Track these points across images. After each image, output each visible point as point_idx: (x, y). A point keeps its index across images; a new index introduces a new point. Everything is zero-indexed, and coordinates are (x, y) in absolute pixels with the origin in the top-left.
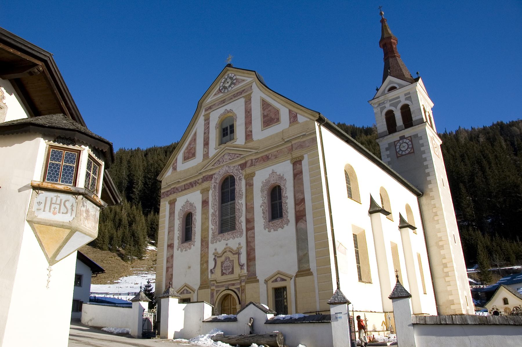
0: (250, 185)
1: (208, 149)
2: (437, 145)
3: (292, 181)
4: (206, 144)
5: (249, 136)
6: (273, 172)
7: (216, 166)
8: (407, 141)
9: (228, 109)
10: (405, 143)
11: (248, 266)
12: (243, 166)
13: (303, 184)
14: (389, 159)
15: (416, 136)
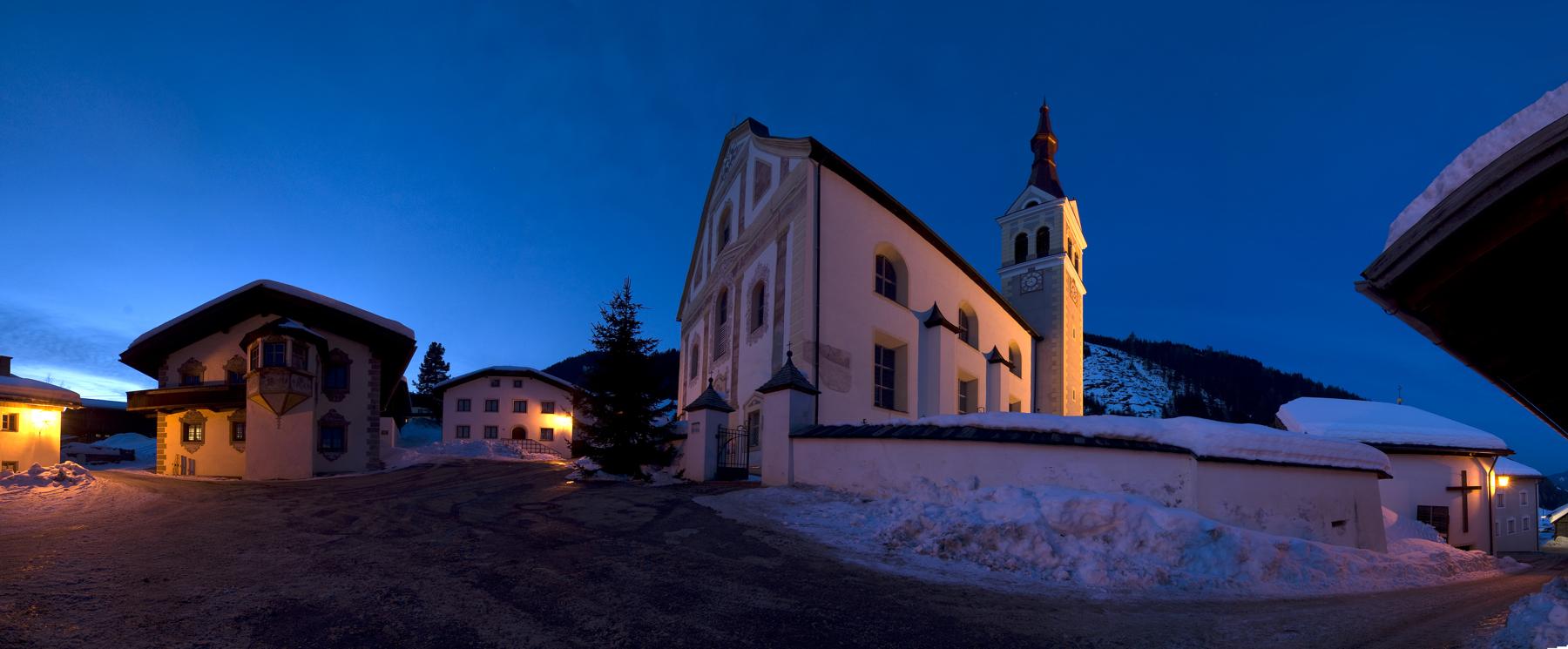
0: (739, 292)
2: (1077, 292)
8: (1038, 275)
12: (734, 271)
15: (1049, 270)
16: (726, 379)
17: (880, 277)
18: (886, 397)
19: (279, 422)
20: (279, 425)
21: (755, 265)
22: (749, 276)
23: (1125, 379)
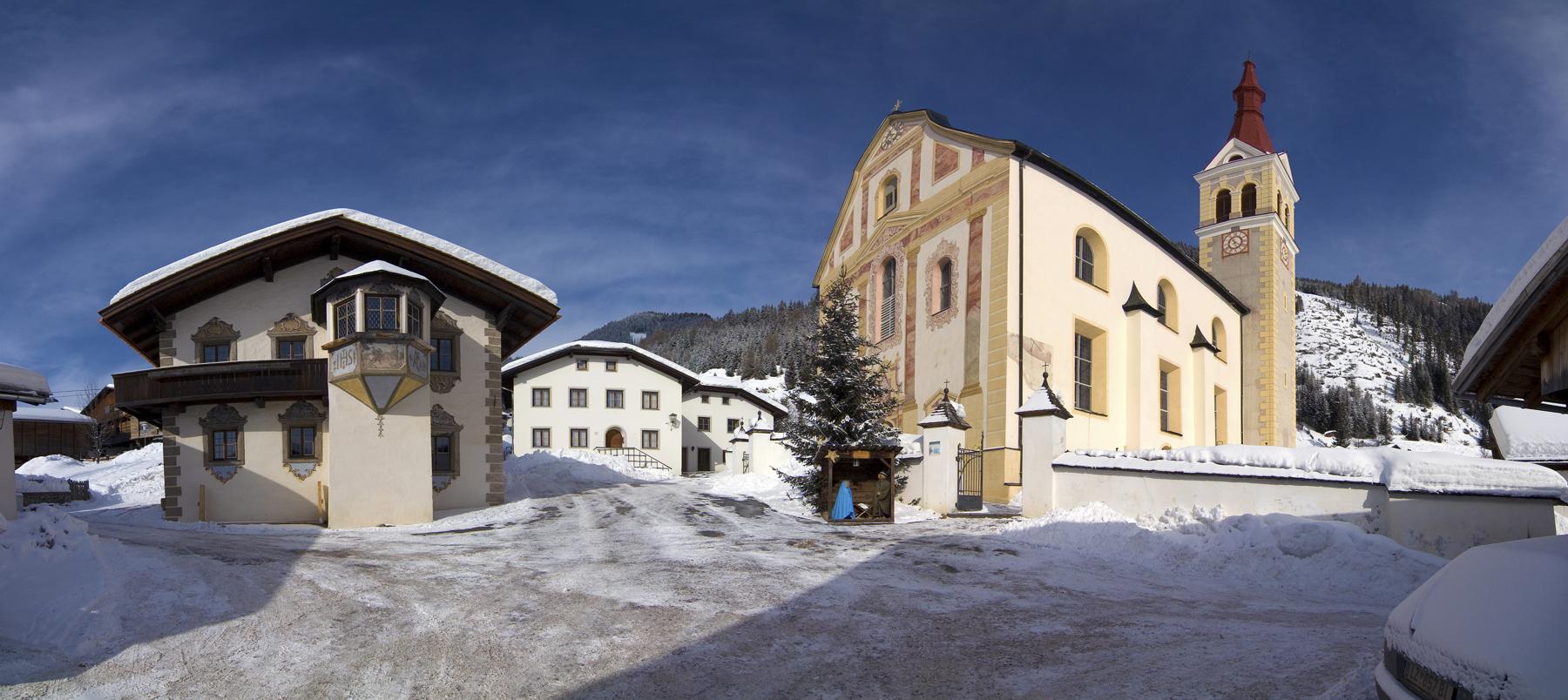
0: (912, 266)
1: (866, 228)
2: (1289, 253)
3: (967, 252)
4: (864, 222)
5: (915, 197)
6: (943, 241)
7: (875, 249)
8: (1242, 235)
9: (891, 169)
10: (1239, 237)
11: (906, 385)
12: (906, 241)
13: (980, 251)
14: (1210, 260)
16: (896, 368)
19: (381, 424)
20: (381, 430)
21: (937, 240)
22: (929, 250)
23: (1348, 341)
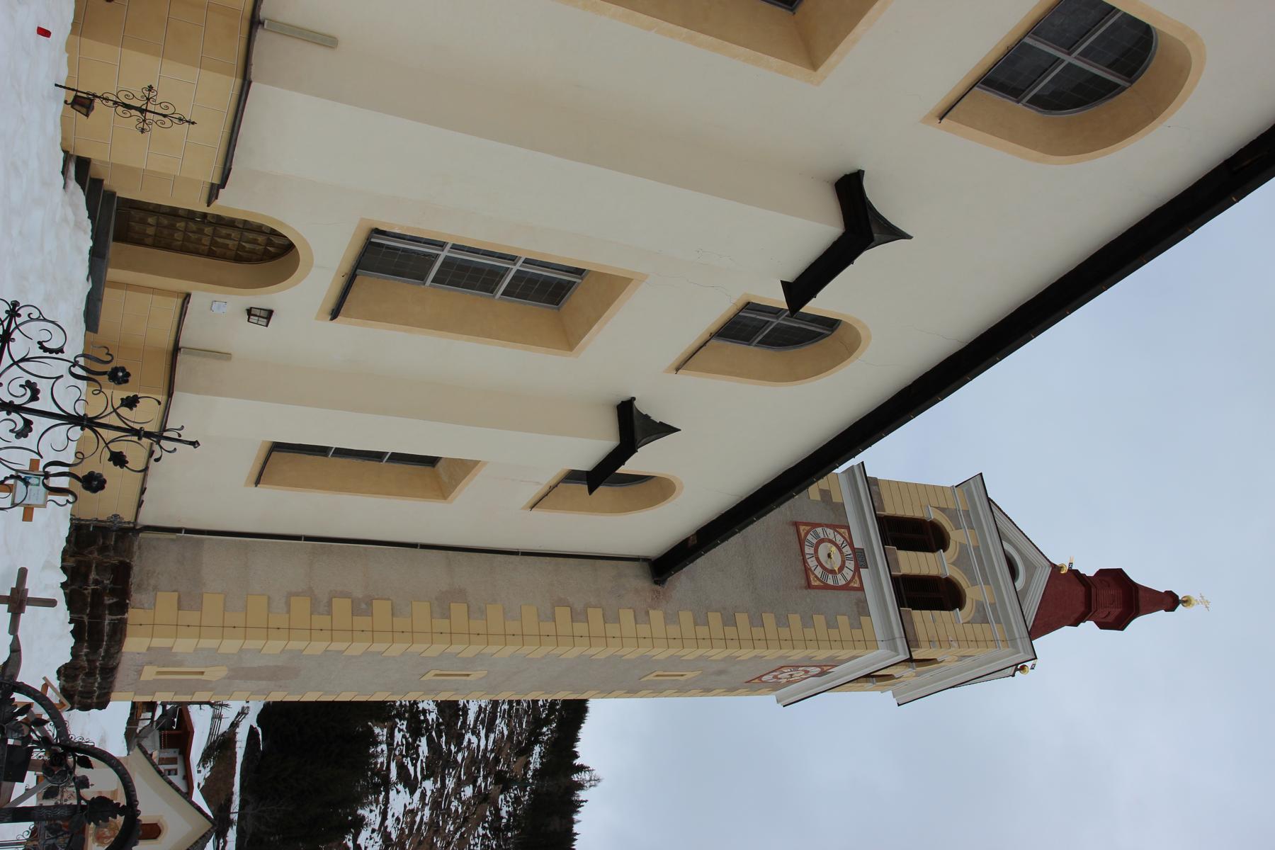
8: (848, 574)
17: (520, 262)
18: (28, 424)
